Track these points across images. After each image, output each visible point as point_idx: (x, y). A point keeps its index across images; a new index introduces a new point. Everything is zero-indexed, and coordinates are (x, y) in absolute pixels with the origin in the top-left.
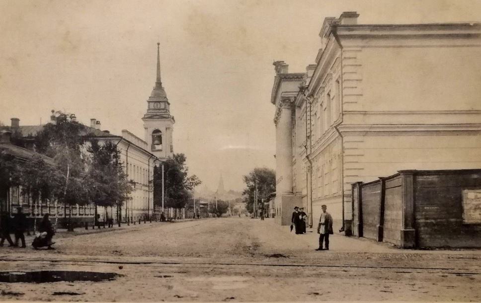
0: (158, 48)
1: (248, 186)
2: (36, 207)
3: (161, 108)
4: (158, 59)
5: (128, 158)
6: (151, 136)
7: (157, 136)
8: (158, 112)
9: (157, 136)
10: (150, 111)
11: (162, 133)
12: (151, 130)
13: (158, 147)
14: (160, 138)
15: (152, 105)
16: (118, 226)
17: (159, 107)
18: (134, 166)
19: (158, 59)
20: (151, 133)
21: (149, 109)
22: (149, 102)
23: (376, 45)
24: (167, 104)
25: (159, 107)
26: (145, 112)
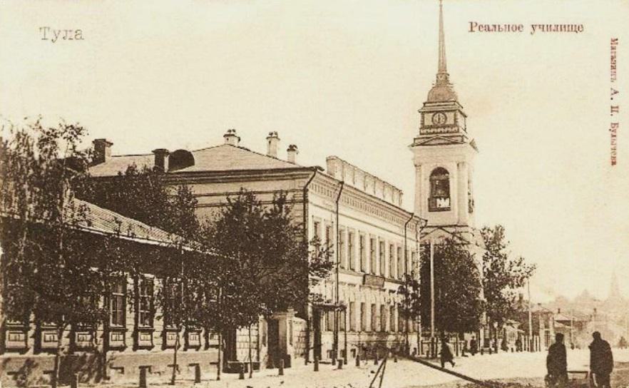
0: (441, 6)
1: (7, 142)
2: (320, 303)
3: (448, 123)
4: (441, 30)
5: (339, 216)
6: (428, 183)
7: (440, 183)
8: (441, 132)
9: (440, 183)
10: (425, 131)
11: (450, 175)
12: (427, 171)
13: (443, 203)
14: (445, 186)
15: (428, 117)
16: (373, 362)
17: (441, 121)
18: (391, 245)
19: (441, 30)
20: (429, 174)
21: (423, 127)
22: (423, 113)
23: (348, 344)
24: (459, 115)
25: (441, 121)
26: (417, 134)
